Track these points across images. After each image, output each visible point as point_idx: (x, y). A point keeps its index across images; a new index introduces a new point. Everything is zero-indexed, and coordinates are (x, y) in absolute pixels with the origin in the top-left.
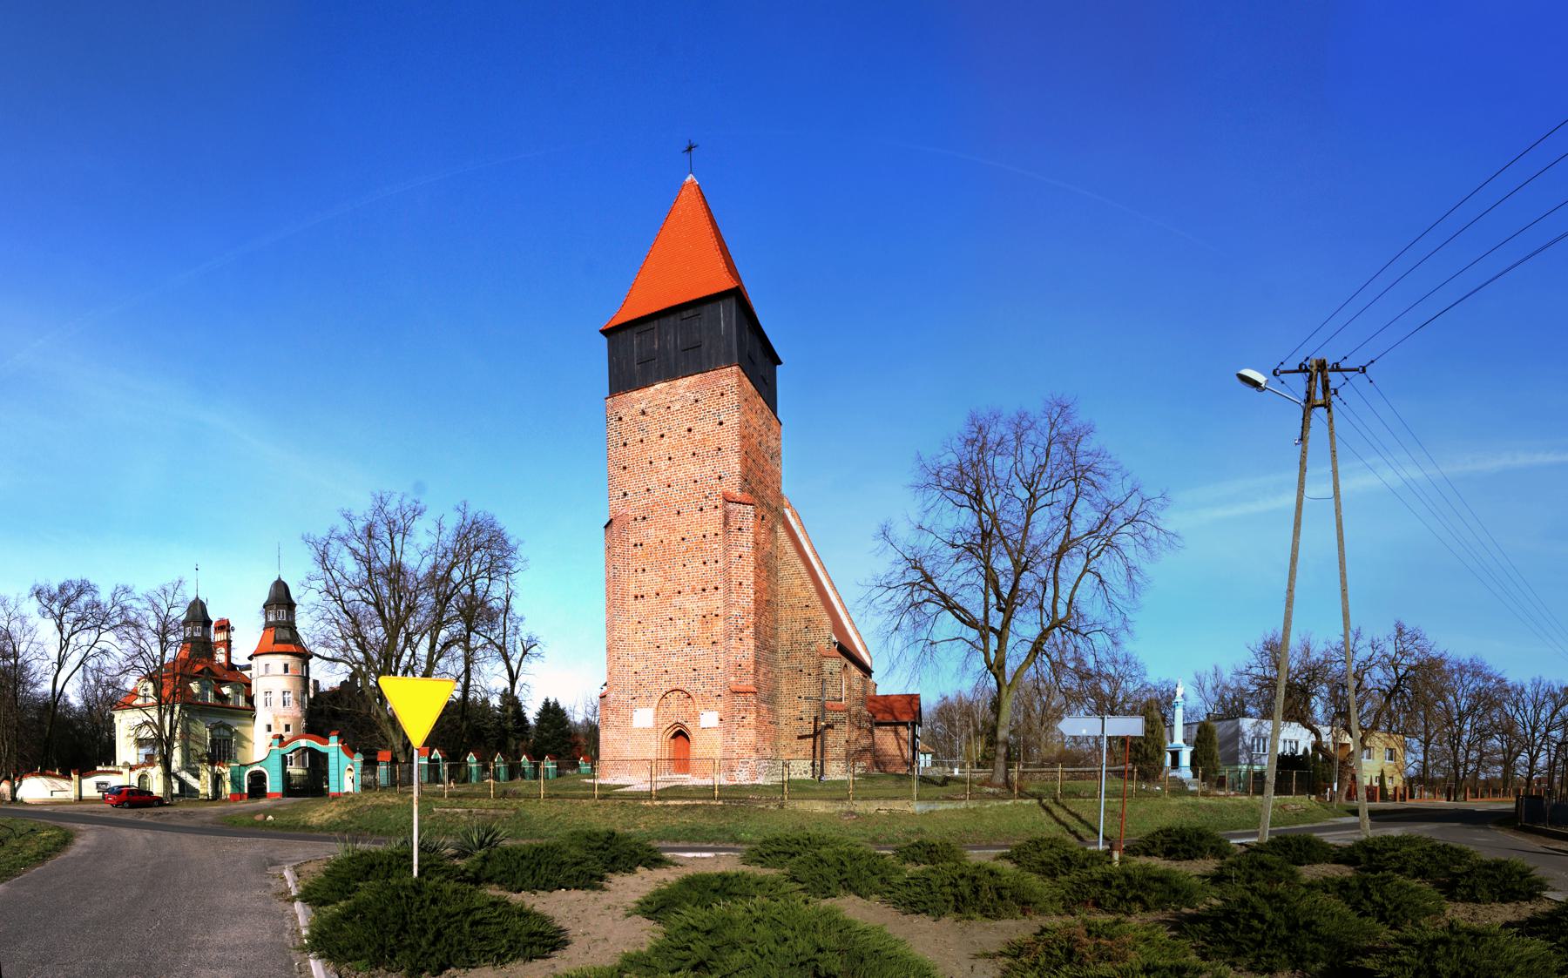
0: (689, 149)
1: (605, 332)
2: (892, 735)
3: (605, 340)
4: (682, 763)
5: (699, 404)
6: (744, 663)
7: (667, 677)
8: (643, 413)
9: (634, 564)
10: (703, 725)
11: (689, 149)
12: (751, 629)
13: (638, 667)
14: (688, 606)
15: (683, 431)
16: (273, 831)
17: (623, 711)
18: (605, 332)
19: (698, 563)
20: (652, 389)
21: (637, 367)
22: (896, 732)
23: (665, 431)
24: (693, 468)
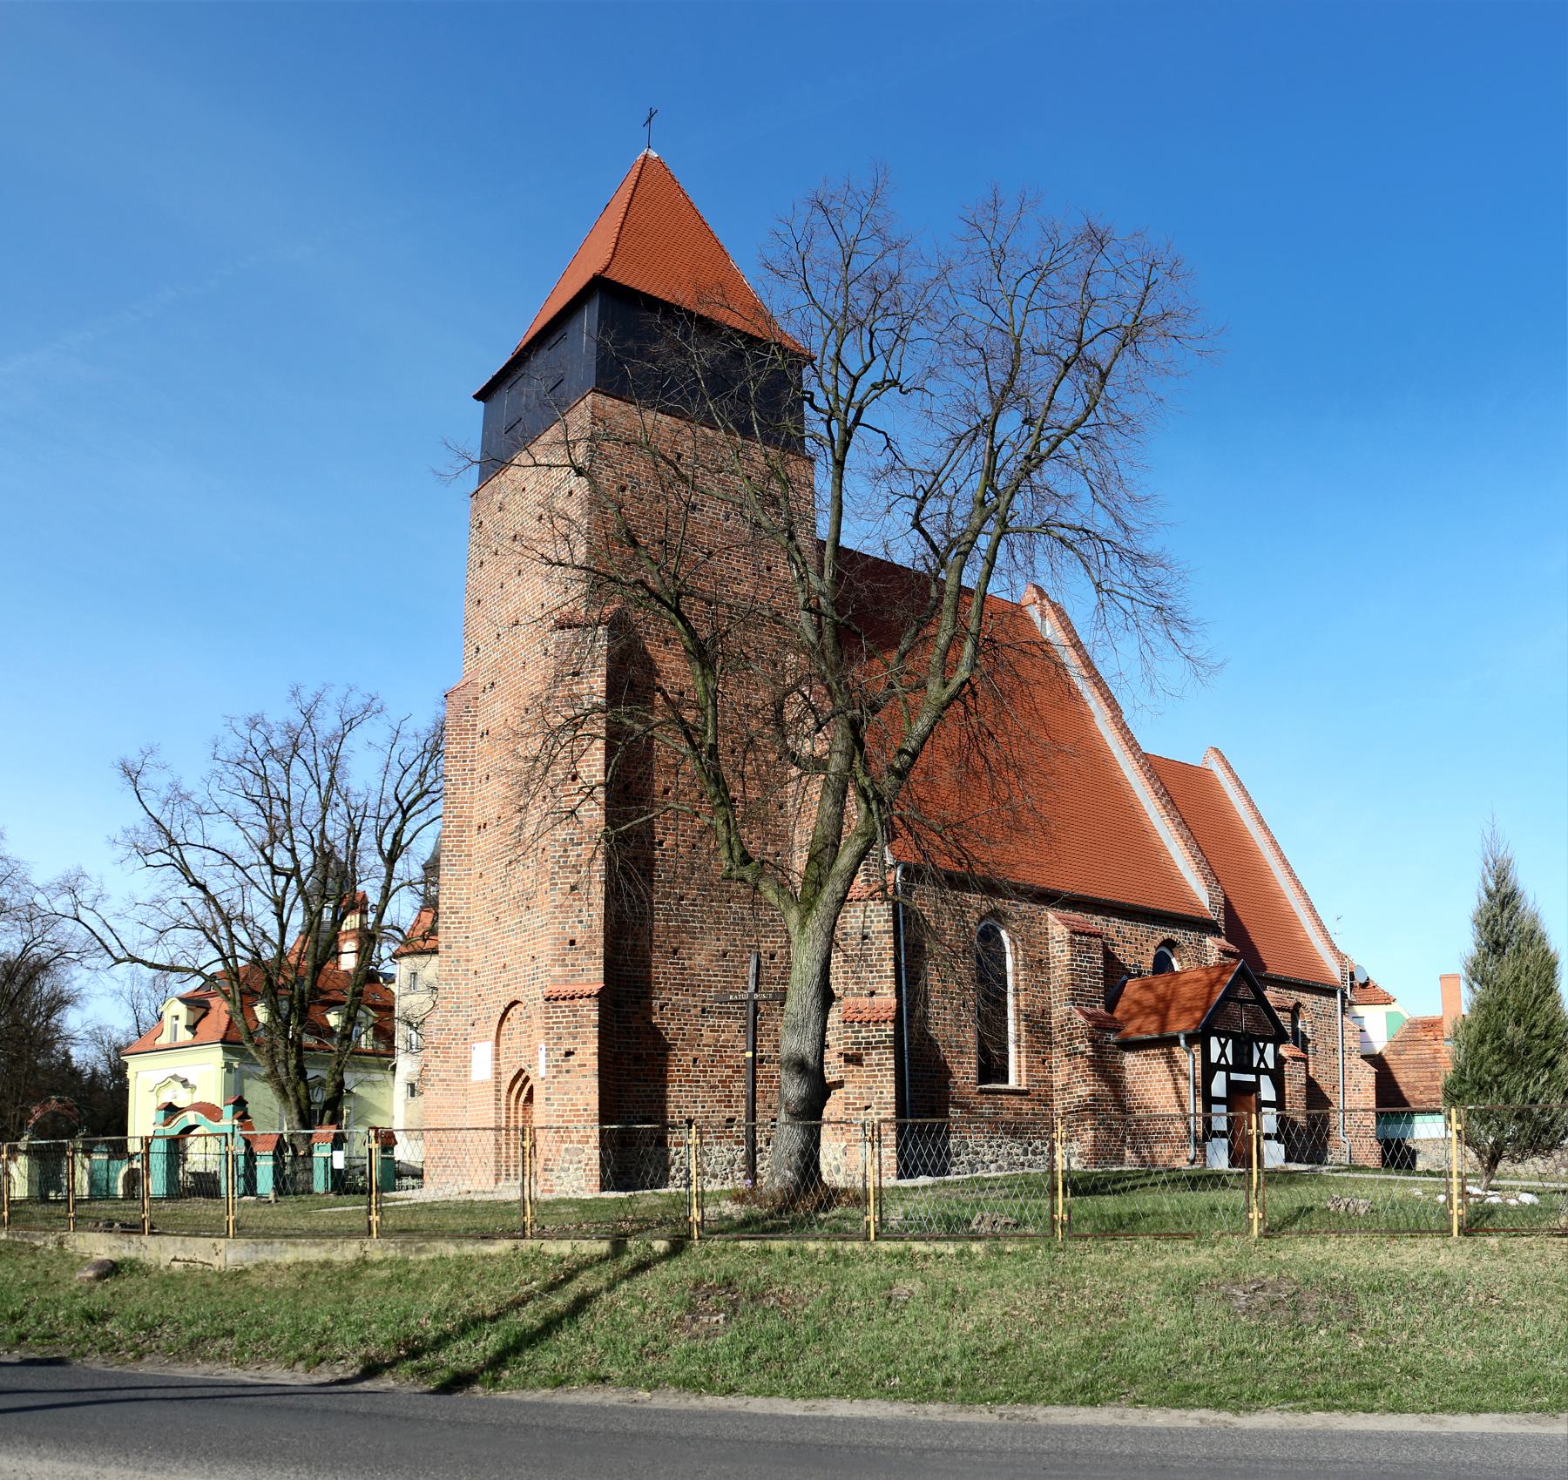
6: (579, 933)
7: (505, 977)
9: (481, 770)
16: (453, 1223)
22: (1171, 1061)
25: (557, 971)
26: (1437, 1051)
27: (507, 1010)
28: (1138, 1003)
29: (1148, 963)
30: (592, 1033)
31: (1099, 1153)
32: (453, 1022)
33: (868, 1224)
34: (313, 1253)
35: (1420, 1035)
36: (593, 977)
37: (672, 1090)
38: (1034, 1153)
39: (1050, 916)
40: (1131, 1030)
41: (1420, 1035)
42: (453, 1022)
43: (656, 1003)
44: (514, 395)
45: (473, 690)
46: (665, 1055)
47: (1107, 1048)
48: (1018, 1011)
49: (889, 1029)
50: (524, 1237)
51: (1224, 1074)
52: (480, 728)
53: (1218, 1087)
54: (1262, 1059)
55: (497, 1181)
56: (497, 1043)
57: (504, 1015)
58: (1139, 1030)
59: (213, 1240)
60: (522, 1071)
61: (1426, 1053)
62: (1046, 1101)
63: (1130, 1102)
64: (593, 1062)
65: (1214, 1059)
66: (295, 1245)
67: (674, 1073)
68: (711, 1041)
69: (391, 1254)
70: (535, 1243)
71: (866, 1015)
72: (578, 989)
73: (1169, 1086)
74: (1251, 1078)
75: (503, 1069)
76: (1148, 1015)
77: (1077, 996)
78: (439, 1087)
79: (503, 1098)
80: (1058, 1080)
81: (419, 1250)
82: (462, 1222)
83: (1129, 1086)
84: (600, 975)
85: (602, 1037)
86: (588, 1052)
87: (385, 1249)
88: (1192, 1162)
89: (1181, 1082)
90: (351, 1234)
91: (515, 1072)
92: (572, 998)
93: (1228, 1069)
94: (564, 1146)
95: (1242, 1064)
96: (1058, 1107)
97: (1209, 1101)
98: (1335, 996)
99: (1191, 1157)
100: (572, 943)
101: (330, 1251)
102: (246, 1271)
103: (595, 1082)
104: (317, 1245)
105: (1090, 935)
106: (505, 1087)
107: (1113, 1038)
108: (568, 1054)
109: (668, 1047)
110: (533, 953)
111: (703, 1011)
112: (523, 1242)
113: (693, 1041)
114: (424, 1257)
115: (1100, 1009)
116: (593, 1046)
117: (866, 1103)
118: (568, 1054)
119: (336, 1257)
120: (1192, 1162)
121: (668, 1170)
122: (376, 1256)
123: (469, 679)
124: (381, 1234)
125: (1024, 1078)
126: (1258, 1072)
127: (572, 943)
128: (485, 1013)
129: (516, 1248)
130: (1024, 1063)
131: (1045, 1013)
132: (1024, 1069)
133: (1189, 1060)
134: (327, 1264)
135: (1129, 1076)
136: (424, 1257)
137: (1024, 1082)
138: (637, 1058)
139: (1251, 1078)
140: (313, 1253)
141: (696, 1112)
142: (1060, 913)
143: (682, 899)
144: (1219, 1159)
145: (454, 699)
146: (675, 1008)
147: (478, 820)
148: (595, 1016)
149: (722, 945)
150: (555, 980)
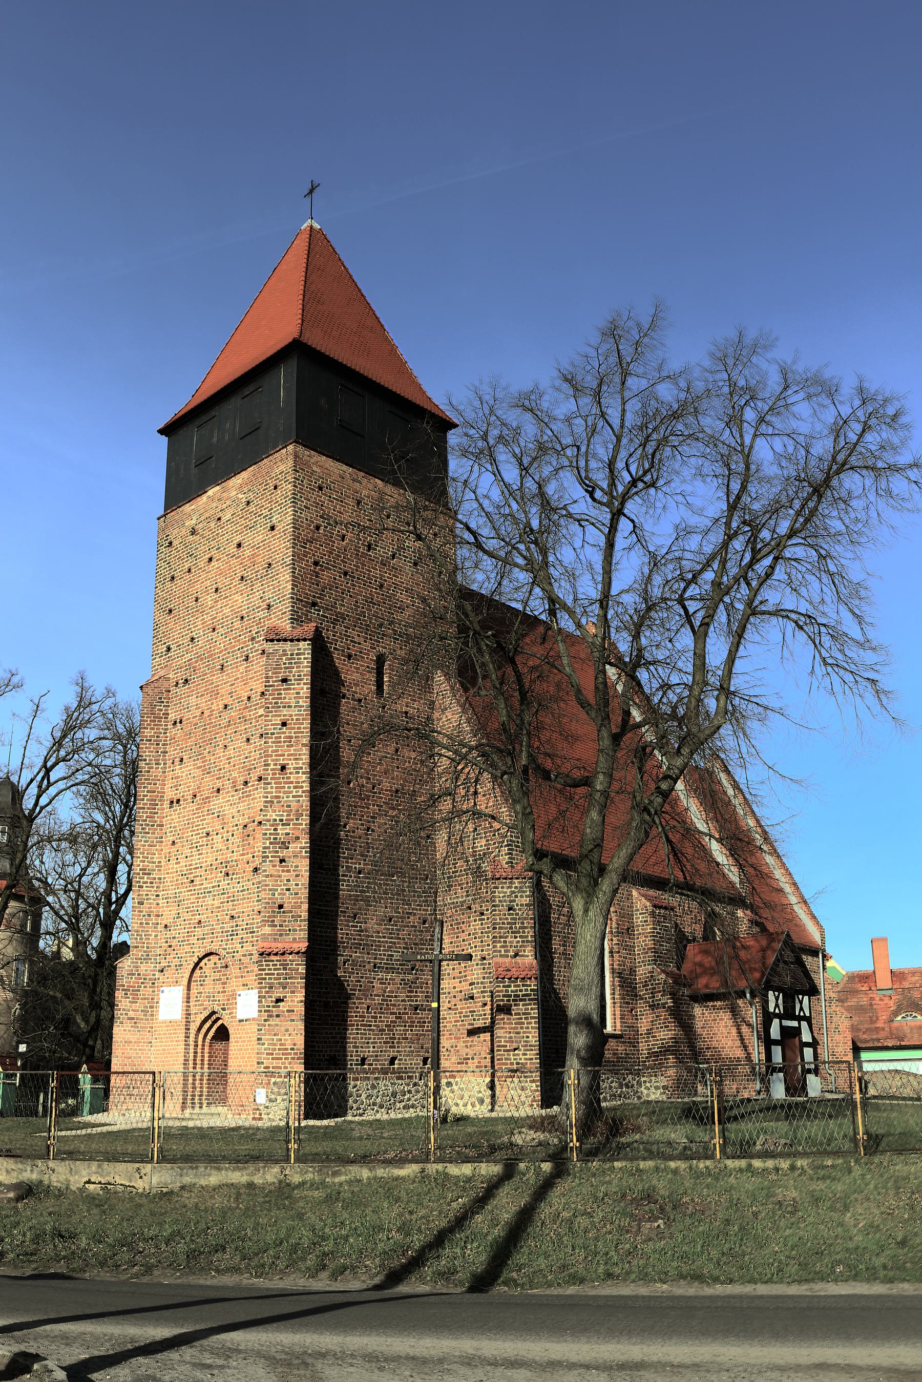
0: (311, 192)
1: (161, 432)
2: (725, 1017)
3: (164, 440)
4: (218, 1082)
5: (252, 508)
6: (289, 901)
7: (199, 932)
8: (193, 532)
9: (172, 752)
10: (240, 1016)
11: (311, 192)
12: (305, 841)
13: (168, 916)
14: (229, 811)
15: (232, 549)
16: (216, 1147)
17: (145, 991)
18: (161, 432)
19: (240, 743)
20: (204, 498)
21: (194, 471)
22: (734, 1011)
23: (213, 552)
24: (239, 600)
25: (267, 930)
26: (872, 999)
27: (200, 960)
28: (700, 965)
29: (699, 934)
30: (300, 982)
31: (682, 1086)
32: (143, 968)
33: (714, 1145)
34: (238, 1177)
35: (858, 986)
36: (299, 938)
37: (351, 1033)
38: (627, 1086)
39: (635, 893)
40: (702, 984)
41: (858, 986)
42: (143, 968)
43: (341, 959)
44: (203, 445)
45: (166, 684)
46: (346, 1003)
47: (682, 999)
48: (613, 971)
49: (533, 985)
50: (427, 1161)
51: (778, 1020)
52: (172, 716)
53: (775, 1032)
54: (801, 1009)
55: (184, 1107)
56: (189, 988)
57: (197, 964)
58: (706, 986)
59: (137, 1165)
60: (214, 1013)
61: (864, 1001)
62: (634, 1043)
63: (700, 1044)
64: (300, 1009)
65: (771, 1010)
66: (219, 1169)
67: (353, 1017)
68: (380, 992)
69: (309, 1176)
70: (440, 1167)
71: (514, 973)
72: (287, 946)
73: (734, 1031)
74: (795, 1024)
75: (193, 1010)
76: (712, 975)
77: (658, 958)
78: (128, 1025)
79: (192, 1036)
80: (643, 1025)
81: (335, 1174)
82: (244, 1148)
83: (699, 1031)
84: (304, 934)
85: (308, 987)
86: (296, 1000)
87: (302, 1173)
88: (759, 1093)
89: (745, 1029)
90: (271, 1160)
91: (206, 1013)
92: (283, 954)
93: (780, 1017)
94: (273, 1080)
95: (789, 1014)
96: (643, 1047)
97: (768, 1043)
98: (817, 956)
99: (758, 1088)
100: (281, 907)
101: (252, 1174)
102: (171, 1193)
103: (301, 1026)
104: (240, 1169)
105: (666, 908)
106: (194, 1027)
107: (686, 992)
108: (279, 1000)
109: (349, 997)
110: (233, 913)
111: (375, 966)
112: (429, 1166)
113: (367, 991)
114: (337, 1180)
115: (672, 967)
116: (301, 995)
117: (515, 1045)
118: (279, 1000)
119: (258, 1180)
120: (759, 1093)
121: (347, 1101)
122: (296, 1179)
123: (162, 673)
124: (297, 1160)
125: (618, 1024)
126: (799, 1019)
127: (281, 907)
128: (176, 962)
129: (423, 1171)
130: (618, 1013)
131: (632, 971)
132: (618, 1016)
133: (752, 1014)
134: (251, 1185)
135: (698, 1025)
136: (337, 1180)
137: (618, 1027)
138: (326, 1005)
139: (795, 1024)
140: (238, 1177)
141: (369, 1051)
142: (644, 890)
143: (360, 872)
144: (779, 1091)
145: (148, 690)
146: (354, 964)
147: (170, 794)
148: (302, 970)
149: (390, 912)
150: (264, 937)
